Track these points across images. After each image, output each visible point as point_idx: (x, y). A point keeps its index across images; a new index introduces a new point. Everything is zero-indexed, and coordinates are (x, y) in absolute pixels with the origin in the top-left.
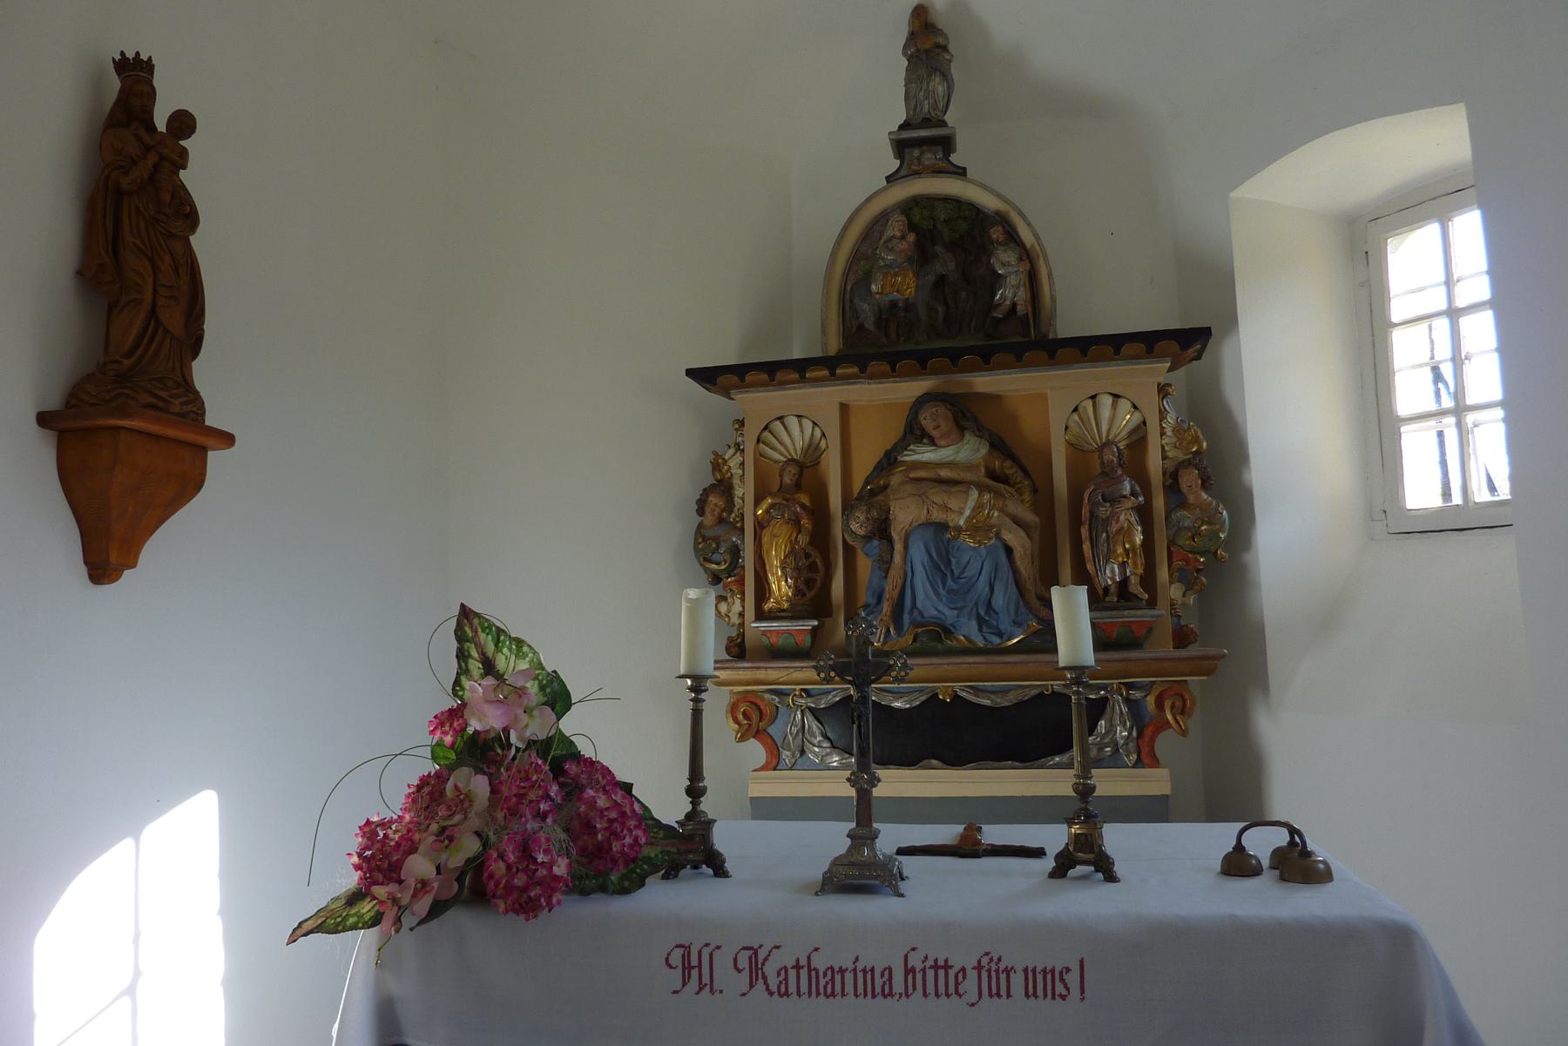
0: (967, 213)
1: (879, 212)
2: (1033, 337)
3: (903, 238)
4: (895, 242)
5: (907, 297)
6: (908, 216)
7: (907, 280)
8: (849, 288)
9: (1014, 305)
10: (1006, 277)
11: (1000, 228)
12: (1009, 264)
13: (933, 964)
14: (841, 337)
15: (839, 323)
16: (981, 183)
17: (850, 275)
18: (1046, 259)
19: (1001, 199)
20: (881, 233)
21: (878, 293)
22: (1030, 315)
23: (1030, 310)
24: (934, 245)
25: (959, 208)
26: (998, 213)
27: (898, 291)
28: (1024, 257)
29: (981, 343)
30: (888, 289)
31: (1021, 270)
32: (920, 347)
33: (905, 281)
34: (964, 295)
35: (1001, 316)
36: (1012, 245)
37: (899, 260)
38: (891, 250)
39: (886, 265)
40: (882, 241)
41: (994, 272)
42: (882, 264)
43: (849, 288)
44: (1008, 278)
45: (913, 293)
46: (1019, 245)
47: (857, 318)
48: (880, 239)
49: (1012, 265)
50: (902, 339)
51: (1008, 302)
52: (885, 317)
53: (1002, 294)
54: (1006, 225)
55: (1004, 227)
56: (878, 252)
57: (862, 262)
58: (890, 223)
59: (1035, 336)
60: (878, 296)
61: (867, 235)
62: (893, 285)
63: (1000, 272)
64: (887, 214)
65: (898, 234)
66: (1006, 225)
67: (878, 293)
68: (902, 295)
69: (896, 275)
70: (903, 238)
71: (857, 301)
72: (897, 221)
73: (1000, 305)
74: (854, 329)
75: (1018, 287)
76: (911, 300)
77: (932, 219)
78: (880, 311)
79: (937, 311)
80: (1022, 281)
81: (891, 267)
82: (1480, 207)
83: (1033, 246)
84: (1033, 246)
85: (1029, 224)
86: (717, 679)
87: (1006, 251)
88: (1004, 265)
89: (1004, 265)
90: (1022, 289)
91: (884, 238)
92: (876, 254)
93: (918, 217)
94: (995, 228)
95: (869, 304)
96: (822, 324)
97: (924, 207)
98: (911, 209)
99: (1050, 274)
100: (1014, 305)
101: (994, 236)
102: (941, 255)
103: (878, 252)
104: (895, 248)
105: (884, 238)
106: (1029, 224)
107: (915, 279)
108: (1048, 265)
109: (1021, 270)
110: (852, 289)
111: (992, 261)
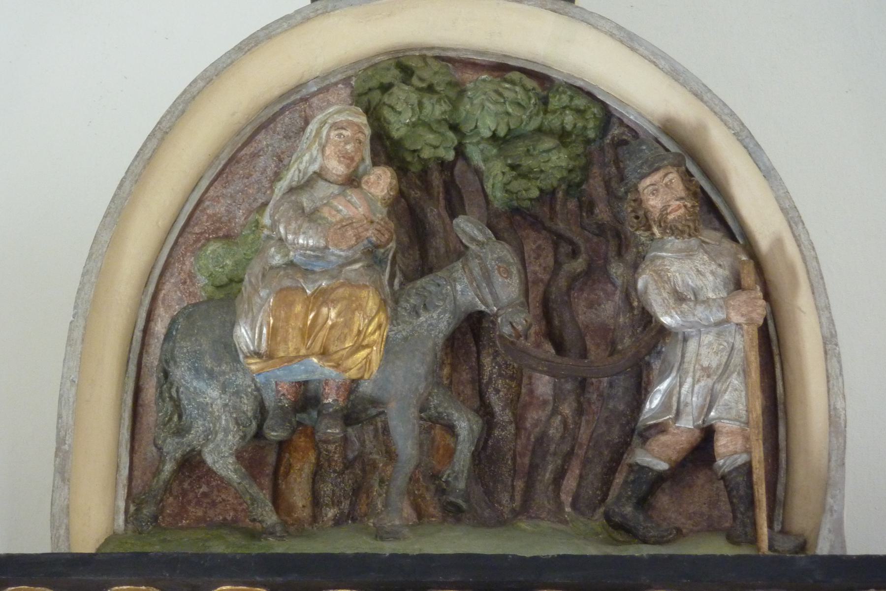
0: (569, 119)
1: (277, 92)
2: (764, 544)
3: (352, 181)
4: (323, 190)
5: (353, 374)
6: (372, 113)
7: (359, 321)
8: (160, 327)
9: (708, 434)
10: (685, 340)
11: (674, 177)
12: (697, 298)
13: (676, 169)
14: (122, 493)
15: (118, 444)
16: (620, 28)
17: (167, 287)
18: (818, 288)
19: (684, 85)
20: (281, 163)
21: (257, 354)
22: (759, 473)
23: (758, 454)
24: (453, 215)
25: (545, 101)
26: (669, 128)
27: (324, 353)
28: (749, 277)
29: (592, 550)
30: (292, 345)
31: (736, 318)
32: (388, 548)
33: (348, 324)
34: (543, 385)
35: (663, 466)
36: (712, 236)
37: (338, 253)
38: (311, 216)
39: (291, 264)
40: (282, 186)
41: (647, 318)
42: (278, 260)
43: (160, 327)
44: (692, 345)
45: (375, 367)
46: (733, 238)
47: (181, 431)
48: (277, 177)
49: (706, 302)
50: (331, 513)
51: (687, 423)
52: (275, 434)
53: (669, 394)
54: (693, 169)
55: (687, 176)
56: (266, 220)
57: (212, 247)
58: (312, 127)
59: (771, 540)
60: (254, 365)
61: (233, 160)
62: (308, 333)
63: (666, 320)
64: (304, 100)
65: (337, 168)
66: (693, 169)
67: (257, 354)
68: (337, 366)
69: (322, 297)
70: (352, 181)
71: (181, 373)
72: (336, 126)
73: (661, 428)
74: (169, 467)
75: (725, 371)
76: (366, 388)
77: (455, 128)
78: (262, 411)
79: (451, 429)
80: (737, 359)
81: (307, 272)
82: (669, 469)
83: (778, 242)
84: (778, 242)
85: (768, 173)
86: (769, 318)
87: (689, 254)
88: (680, 298)
89: (680, 298)
90: (735, 381)
91: (291, 177)
92: (257, 224)
93: (407, 117)
94: (656, 177)
95: (224, 389)
96: (60, 441)
97: (430, 89)
98: (386, 88)
99: (829, 341)
100: (708, 434)
101: (654, 203)
102: (473, 247)
103: (266, 220)
104: (325, 212)
105: (291, 177)
106: (768, 173)
107: (382, 317)
108: (823, 309)
109: (736, 318)
110: (168, 336)
111: (640, 284)
